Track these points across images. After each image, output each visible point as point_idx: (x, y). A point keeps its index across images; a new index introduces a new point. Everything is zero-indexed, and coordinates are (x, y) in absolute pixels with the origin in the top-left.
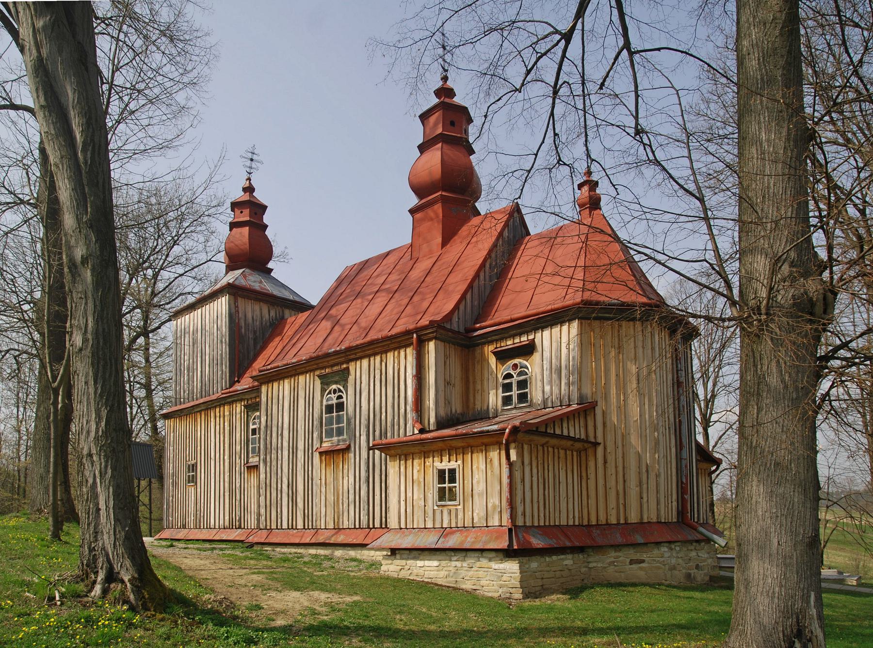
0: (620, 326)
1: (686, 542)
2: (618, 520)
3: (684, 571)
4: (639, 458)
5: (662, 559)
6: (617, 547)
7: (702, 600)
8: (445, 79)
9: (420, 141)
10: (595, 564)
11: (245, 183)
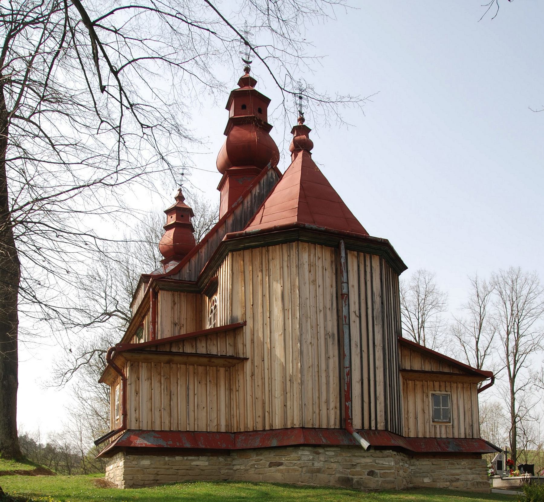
0: (268, 251)
1: (342, 447)
2: (264, 426)
3: (338, 475)
4: (284, 369)
5: (299, 462)
6: (258, 450)
7: (133, 492)
8: (247, 70)
9: (291, 130)
10: (238, 467)
11: (176, 193)
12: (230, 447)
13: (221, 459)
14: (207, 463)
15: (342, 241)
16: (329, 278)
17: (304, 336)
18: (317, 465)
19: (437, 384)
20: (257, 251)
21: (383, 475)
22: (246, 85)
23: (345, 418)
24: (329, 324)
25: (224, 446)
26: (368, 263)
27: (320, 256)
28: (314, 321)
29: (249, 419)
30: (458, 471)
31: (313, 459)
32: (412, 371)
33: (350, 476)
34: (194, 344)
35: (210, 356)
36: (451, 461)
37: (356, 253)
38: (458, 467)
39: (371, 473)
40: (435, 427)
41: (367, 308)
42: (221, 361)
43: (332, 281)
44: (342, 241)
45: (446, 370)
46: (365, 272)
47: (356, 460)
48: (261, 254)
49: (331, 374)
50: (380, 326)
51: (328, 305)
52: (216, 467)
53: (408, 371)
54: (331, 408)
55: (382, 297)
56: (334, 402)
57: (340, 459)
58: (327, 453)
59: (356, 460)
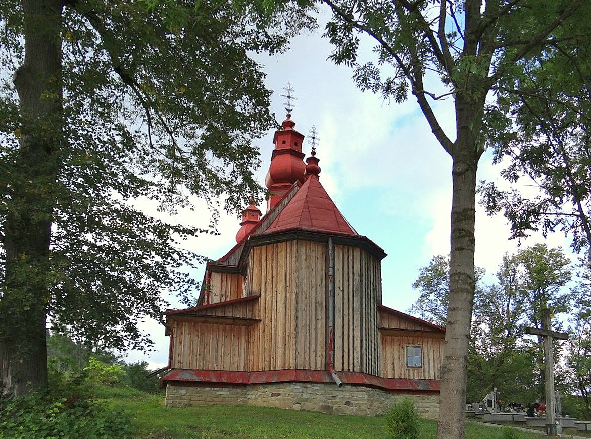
3: (321, 404)
5: (291, 394)
8: (289, 116)
10: (250, 396)
12: (245, 382)
13: (239, 390)
14: (228, 393)
15: (330, 238)
16: (321, 265)
17: (299, 305)
18: (305, 396)
19: (410, 339)
20: (270, 246)
21: (357, 405)
22: (287, 126)
23: (329, 365)
24: (319, 296)
25: (240, 381)
26: (351, 253)
27: (314, 249)
28: (308, 293)
29: (261, 364)
30: (427, 405)
31: (302, 392)
32: (389, 329)
33: (331, 405)
34: (223, 310)
35: (234, 319)
36: (421, 396)
37: (341, 246)
38: (427, 401)
39: (348, 403)
40: (409, 371)
41: (349, 285)
42: (242, 322)
43: (322, 266)
44: (330, 238)
45: (418, 329)
46: (348, 259)
47: (335, 394)
48: (306, 245)
49: (319, 331)
50: (359, 297)
51: (319, 283)
52: (235, 396)
53: (387, 329)
54: (318, 355)
55: (361, 276)
56: (320, 351)
57: (323, 392)
58: (313, 387)
59: (335, 394)
